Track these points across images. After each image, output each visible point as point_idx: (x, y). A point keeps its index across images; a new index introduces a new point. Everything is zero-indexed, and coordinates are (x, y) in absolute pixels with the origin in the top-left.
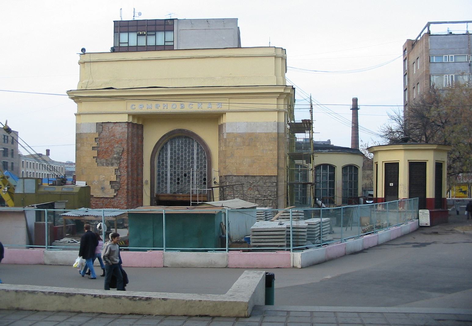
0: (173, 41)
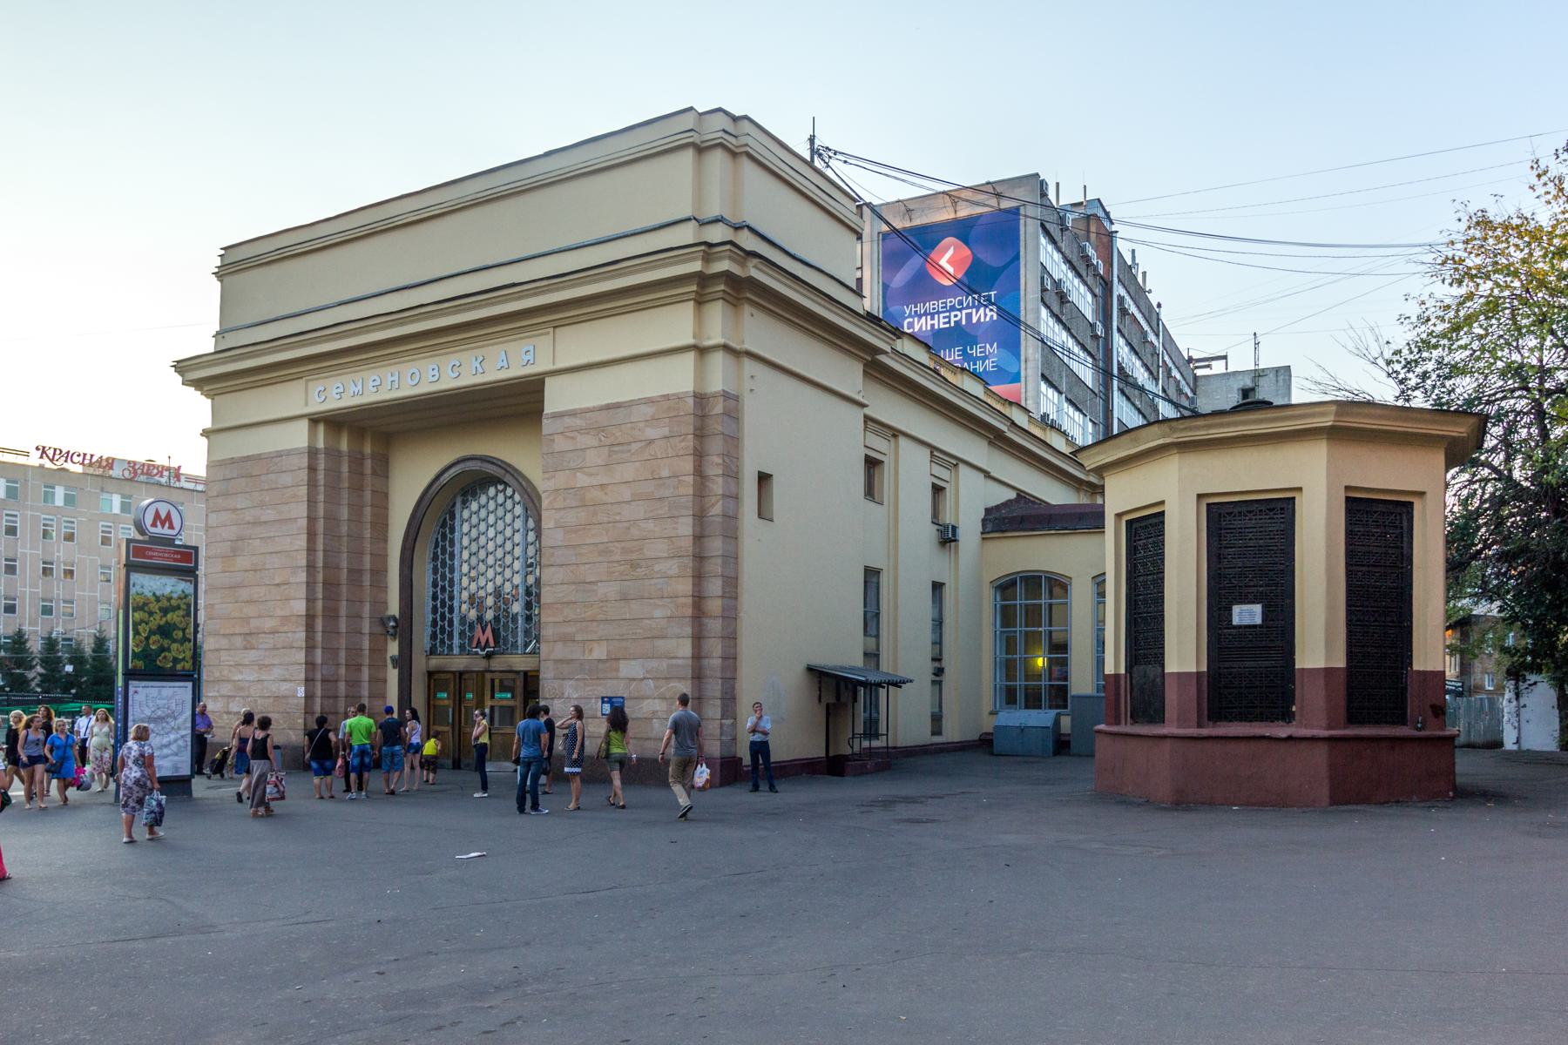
0: (861, 268)
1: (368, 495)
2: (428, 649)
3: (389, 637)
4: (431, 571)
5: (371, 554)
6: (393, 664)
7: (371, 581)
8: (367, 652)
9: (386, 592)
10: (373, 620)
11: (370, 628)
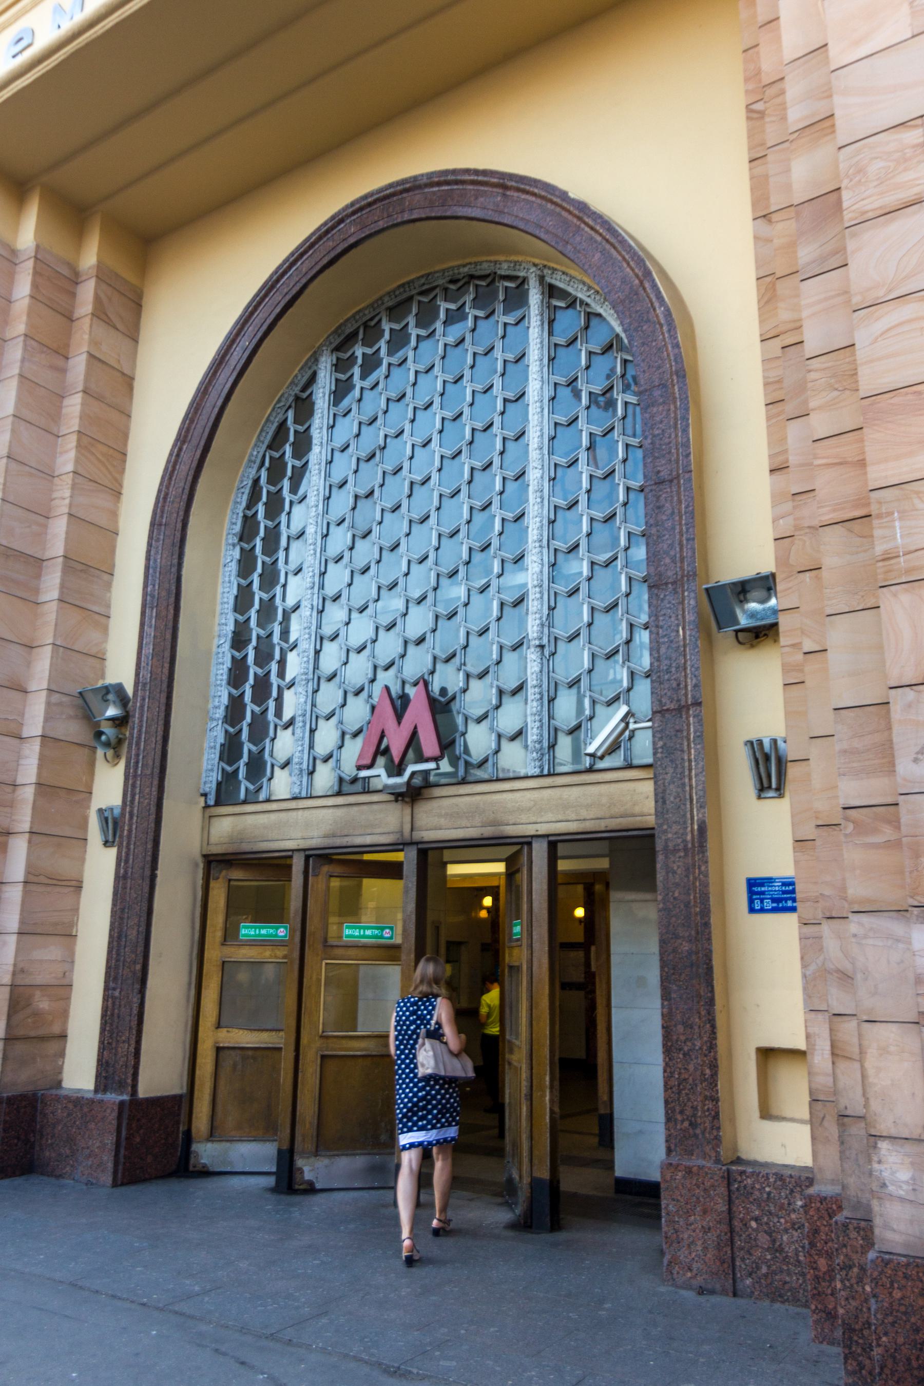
1: (78, 365)
2: (211, 787)
3: (100, 752)
4: (233, 567)
5: (70, 515)
6: (104, 831)
7: (62, 586)
8: (28, 793)
9: (105, 630)
10: (56, 698)
11: (47, 719)
